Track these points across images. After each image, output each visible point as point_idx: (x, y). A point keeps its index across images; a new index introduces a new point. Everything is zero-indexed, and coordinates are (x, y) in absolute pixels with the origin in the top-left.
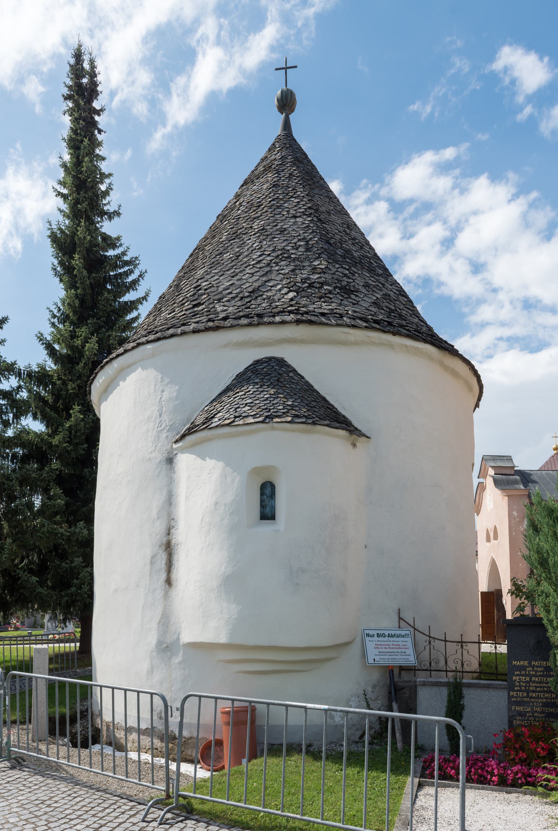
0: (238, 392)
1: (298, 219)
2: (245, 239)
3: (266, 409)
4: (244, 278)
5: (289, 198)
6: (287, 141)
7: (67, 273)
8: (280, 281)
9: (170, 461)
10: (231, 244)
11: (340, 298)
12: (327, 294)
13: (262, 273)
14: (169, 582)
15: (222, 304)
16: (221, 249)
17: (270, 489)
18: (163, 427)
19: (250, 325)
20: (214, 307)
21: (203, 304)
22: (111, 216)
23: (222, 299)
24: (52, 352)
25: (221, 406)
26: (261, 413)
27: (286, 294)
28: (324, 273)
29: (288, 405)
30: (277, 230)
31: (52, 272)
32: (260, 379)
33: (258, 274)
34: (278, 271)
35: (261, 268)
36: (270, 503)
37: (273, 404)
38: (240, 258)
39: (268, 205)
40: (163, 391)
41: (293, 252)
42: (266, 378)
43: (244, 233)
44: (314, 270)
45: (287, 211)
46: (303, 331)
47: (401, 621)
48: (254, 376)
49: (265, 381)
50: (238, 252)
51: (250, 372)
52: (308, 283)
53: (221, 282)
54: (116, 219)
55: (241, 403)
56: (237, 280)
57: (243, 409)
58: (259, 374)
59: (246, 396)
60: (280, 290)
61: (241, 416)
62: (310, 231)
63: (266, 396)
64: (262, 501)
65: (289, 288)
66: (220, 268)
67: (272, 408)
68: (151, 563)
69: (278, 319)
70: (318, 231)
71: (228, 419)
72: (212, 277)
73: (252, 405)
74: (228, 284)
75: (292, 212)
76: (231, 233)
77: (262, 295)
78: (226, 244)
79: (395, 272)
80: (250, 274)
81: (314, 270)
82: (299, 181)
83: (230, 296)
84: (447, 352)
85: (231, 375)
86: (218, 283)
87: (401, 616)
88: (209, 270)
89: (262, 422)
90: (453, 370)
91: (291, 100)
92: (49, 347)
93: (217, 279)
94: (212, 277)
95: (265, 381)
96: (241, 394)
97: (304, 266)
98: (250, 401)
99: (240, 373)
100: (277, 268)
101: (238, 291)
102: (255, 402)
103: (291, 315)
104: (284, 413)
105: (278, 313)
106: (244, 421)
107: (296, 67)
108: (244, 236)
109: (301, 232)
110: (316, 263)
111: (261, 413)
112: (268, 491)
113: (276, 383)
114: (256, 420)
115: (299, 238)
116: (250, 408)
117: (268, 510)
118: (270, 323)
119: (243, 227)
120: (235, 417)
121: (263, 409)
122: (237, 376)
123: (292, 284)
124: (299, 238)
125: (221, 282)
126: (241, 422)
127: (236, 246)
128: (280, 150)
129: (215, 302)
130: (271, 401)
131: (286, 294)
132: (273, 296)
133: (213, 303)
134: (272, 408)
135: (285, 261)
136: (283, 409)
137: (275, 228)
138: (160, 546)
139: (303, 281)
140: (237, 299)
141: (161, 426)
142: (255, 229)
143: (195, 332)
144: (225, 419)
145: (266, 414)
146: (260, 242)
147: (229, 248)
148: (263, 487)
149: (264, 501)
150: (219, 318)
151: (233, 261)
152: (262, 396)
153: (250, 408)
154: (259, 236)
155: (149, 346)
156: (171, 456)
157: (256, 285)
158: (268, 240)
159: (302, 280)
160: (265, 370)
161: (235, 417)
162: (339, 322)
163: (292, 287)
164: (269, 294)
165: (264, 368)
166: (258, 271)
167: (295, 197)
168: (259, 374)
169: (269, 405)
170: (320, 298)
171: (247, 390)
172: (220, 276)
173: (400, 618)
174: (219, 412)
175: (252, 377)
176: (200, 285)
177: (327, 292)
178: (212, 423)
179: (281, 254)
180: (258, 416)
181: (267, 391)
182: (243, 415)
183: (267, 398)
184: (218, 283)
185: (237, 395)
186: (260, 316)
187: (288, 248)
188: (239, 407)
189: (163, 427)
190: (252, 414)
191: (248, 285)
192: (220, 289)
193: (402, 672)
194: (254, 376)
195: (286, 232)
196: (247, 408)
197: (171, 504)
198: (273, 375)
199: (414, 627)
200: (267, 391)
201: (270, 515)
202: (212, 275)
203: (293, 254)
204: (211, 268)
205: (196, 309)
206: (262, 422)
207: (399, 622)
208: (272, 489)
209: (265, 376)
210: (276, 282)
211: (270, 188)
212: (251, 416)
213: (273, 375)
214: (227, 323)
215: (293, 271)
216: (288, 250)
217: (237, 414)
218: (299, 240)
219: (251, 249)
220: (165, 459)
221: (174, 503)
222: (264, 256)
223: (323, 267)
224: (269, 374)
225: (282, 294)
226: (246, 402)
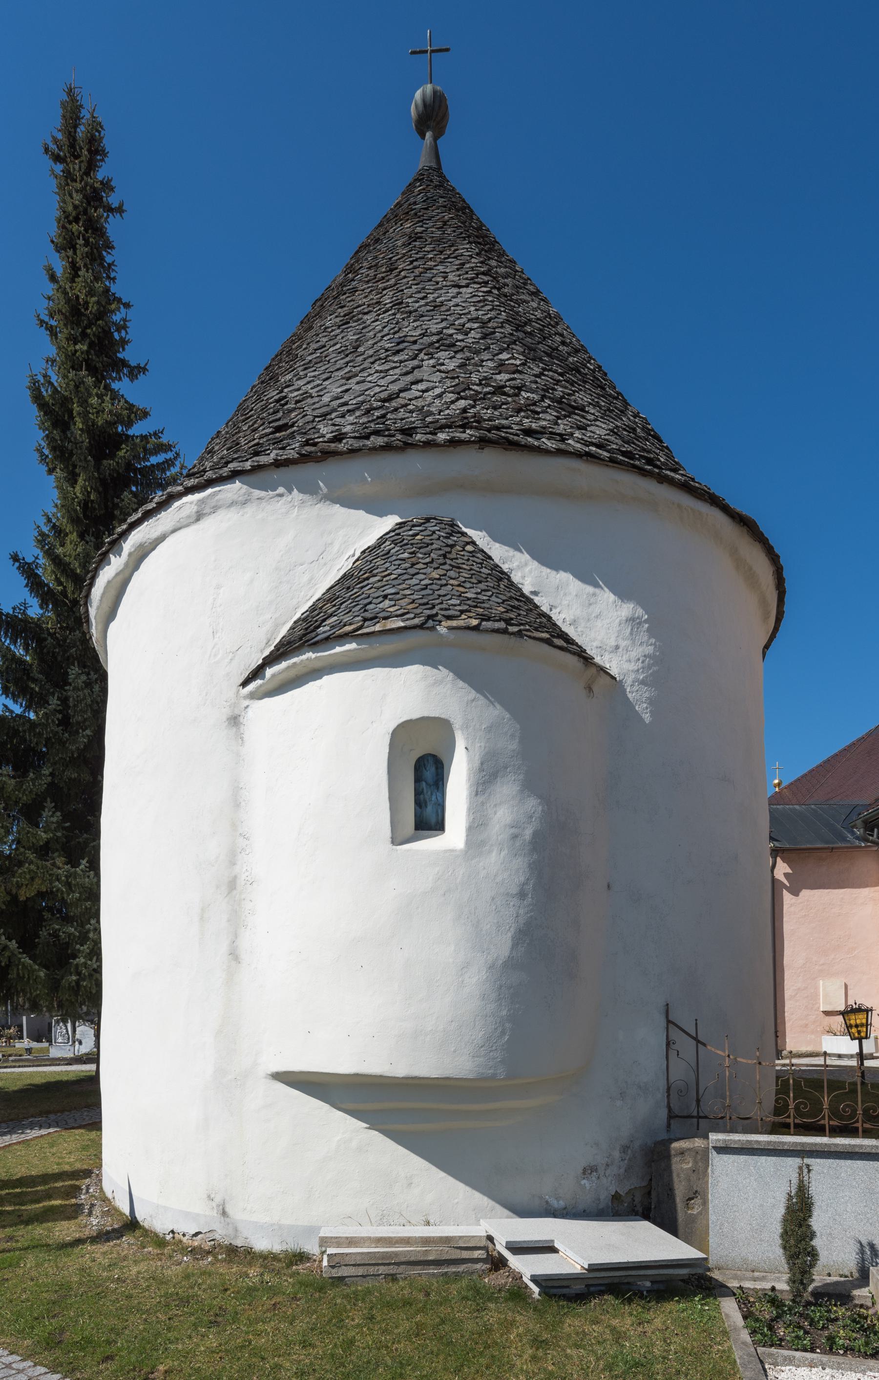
0: (368, 579)
1: (463, 290)
2: (368, 322)
3: (427, 604)
4: (369, 379)
5: (445, 258)
6: (433, 178)
7: (61, 456)
8: (440, 382)
9: (235, 721)
10: (342, 332)
11: (555, 414)
12: (529, 405)
13: (405, 370)
14: (234, 955)
15: (330, 422)
16: (325, 340)
17: (433, 769)
18: (219, 656)
19: (387, 448)
20: (314, 428)
21: (292, 426)
22: (136, 372)
23: (330, 414)
24: (35, 583)
25: (334, 606)
26: (418, 611)
27: (453, 402)
28: (520, 372)
29: (469, 599)
30: (427, 304)
31: (37, 455)
32: (410, 553)
33: (397, 371)
34: (434, 367)
35: (401, 362)
36: (434, 798)
37: (440, 596)
38: (361, 349)
39: (408, 268)
40: (218, 587)
41: (460, 337)
42: (421, 550)
43: (366, 311)
44: (501, 367)
45: (443, 277)
46: (491, 463)
47: (671, 1025)
48: (397, 549)
49: (420, 556)
50: (357, 340)
51: (388, 543)
52: (493, 386)
53: (325, 388)
54: (141, 377)
55: (376, 595)
56: (358, 383)
57: (381, 606)
58: (407, 544)
59: (384, 583)
60: (440, 396)
61: (376, 617)
62: (489, 307)
63: (423, 583)
64: (418, 793)
65: (459, 393)
66: (323, 368)
67: (437, 601)
68: (202, 918)
69: (442, 436)
70: (502, 309)
71: (351, 624)
72: (308, 383)
73: (398, 596)
74: (340, 390)
75: (451, 277)
76: (342, 314)
77: (406, 405)
78: (333, 331)
79: (437, 683)
80: (381, 372)
81: (501, 367)
82: (462, 233)
83: (346, 408)
84: (745, 529)
85: (351, 553)
86: (321, 390)
87: (670, 1018)
88: (301, 373)
89: (421, 627)
90: (751, 569)
91: (440, 106)
92: (28, 571)
93: (318, 385)
94: (308, 383)
95: (420, 556)
96: (372, 580)
97: (483, 361)
98: (393, 591)
99: (369, 547)
100: (432, 362)
101: (360, 399)
102: (402, 592)
103: (468, 431)
104: (462, 612)
105: (442, 428)
106: (385, 626)
107: (447, 50)
108: (365, 317)
109: (473, 309)
110: (504, 356)
111: (418, 611)
112: (429, 773)
113: (441, 561)
114: (408, 623)
115: (469, 316)
116: (393, 603)
117: (430, 810)
118: (428, 444)
119: (364, 304)
120: (365, 620)
121: (420, 605)
122: (364, 552)
123: (463, 386)
124: (469, 316)
125: (325, 388)
126: (378, 628)
127: (351, 333)
128: (424, 189)
129: (317, 419)
130: (434, 591)
131: (453, 402)
132: (429, 405)
133: (313, 421)
134: (437, 601)
135: (446, 351)
136: (459, 605)
137: (422, 302)
138: (218, 887)
139: (484, 381)
140: (358, 413)
141: (215, 655)
142: (386, 304)
143: (278, 464)
144: (345, 625)
145: (428, 612)
146: (396, 324)
147: (340, 337)
148: (420, 765)
149: (422, 792)
150: (326, 439)
151: (347, 356)
152: (414, 581)
153: (393, 603)
154: (394, 314)
155: (189, 498)
156: (237, 712)
157: (395, 388)
158: (412, 319)
159: (480, 380)
160: (419, 537)
161: (365, 620)
162: (563, 446)
163: (464, 391)
164: (419, 403)
165: (417, 534)
166: (396, 367)
167: (455, 257)
168: (407, 544)
169: (431, 597)
170: (519, 411)
171: (386, 573)
172: (325, 380)
173: (669, 1022)
174: (331, 615)
175: (393, 551)
176: (285, 397)
177: (529, 402)
178: (317, 635)
179: (438, 341)
180: (412, 616)
181: (425, 574)
182: (381, 615)
183: (427, 585)
184: (321, 390)
185: (366, 583)
186: (408, 432)
187: (451, 331)
188: (370, 603)
189: (219, 656)
190: (399, 612)
191: (377, 389)
192: (326, 399)
193: (672, 1121)
194: (397, 549)
195: (443, 308)
196: (387, 603)
197: (237, 805)
198: (434, 546)
199: (696, 1039)
200: (425, 574)
201: (433, 820)
202: (308, 379)
203: (458, 341)
204: (305, 369)
205: (278, 435)
206: (421, 627)
207: (667, 1028)
208: (437, 768)
209: (420, 548)
210: (432, 384)
211: (410, 244)
212: (397, 616)
213: (434, 546)
214: (342, 446)
215: (461, 366)
216: (451, 335)
217: (368, 615)
218: (469, 320)
219: (380, 335)
220: (224, 718)
221: (243, 804)
222: (406, 344)
223: (518, 362)
224: (428, 545)
225: (446, 403)
226: (385, 593)
